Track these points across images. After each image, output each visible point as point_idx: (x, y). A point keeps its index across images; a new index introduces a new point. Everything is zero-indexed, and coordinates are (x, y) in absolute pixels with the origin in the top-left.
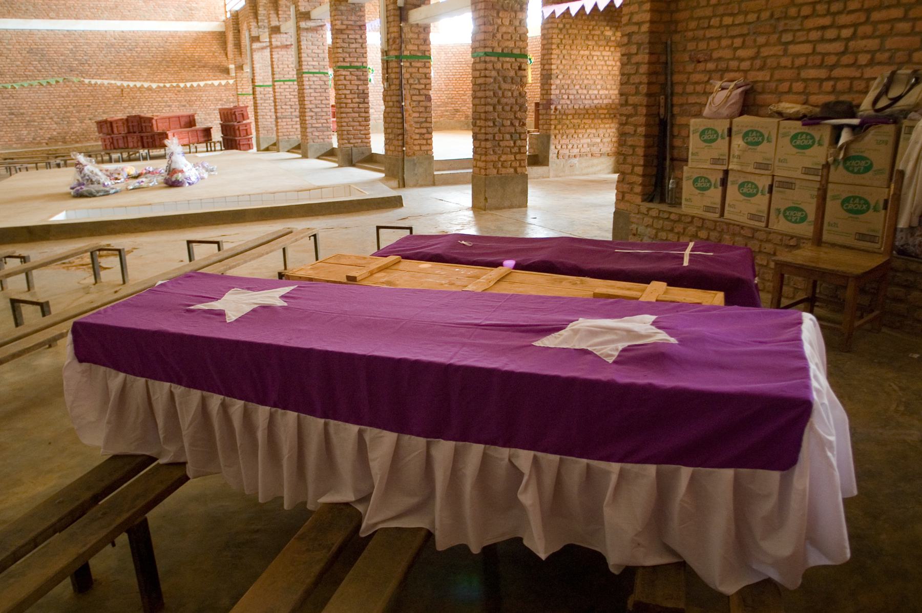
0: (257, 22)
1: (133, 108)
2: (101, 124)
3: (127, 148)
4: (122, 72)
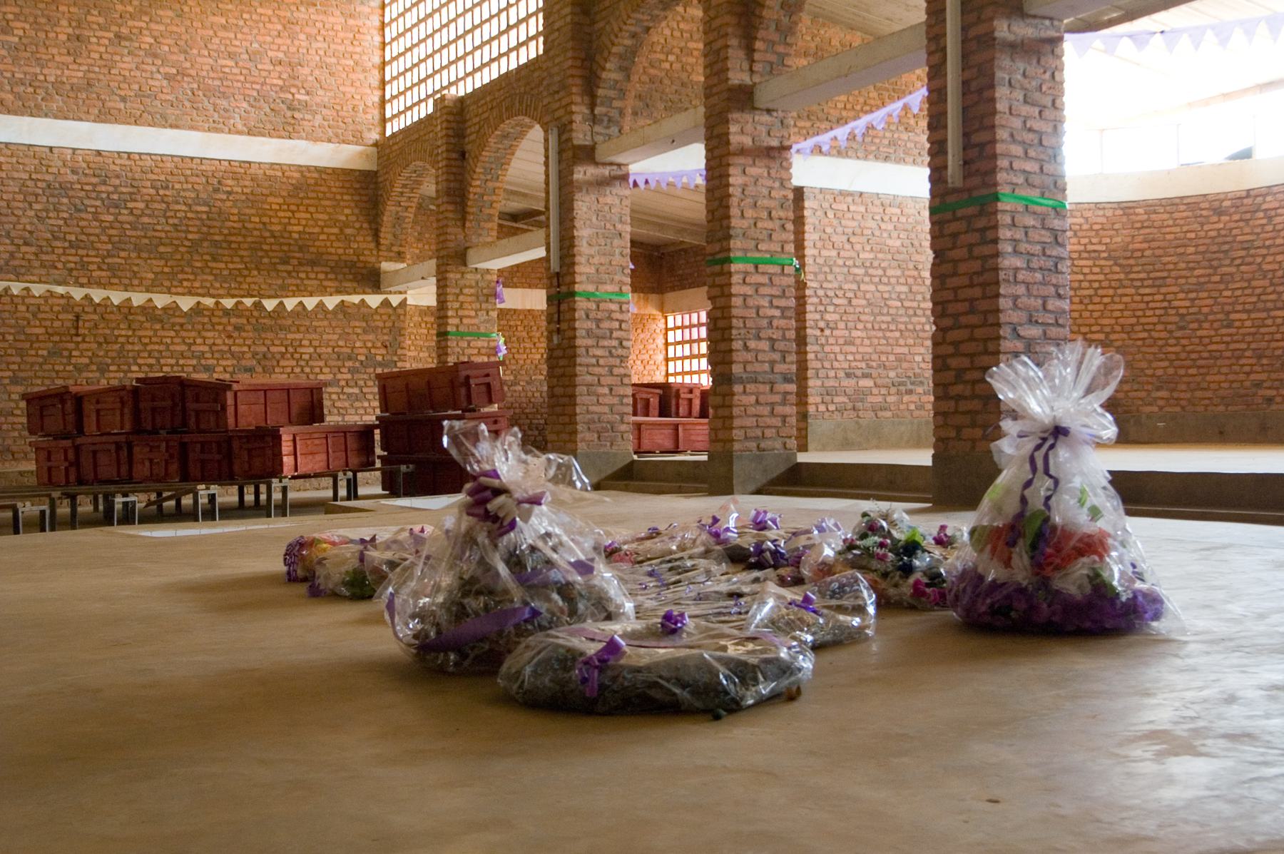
0: (592, 106)
1: (103, 369)
2: (40, 404)
3: (130, 479)
4: (84, 266)
